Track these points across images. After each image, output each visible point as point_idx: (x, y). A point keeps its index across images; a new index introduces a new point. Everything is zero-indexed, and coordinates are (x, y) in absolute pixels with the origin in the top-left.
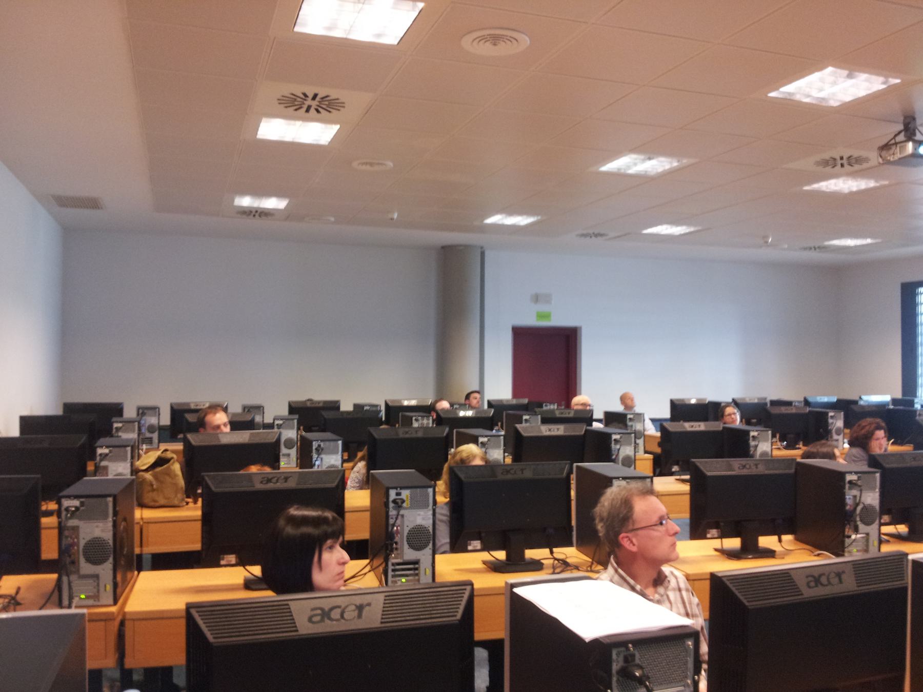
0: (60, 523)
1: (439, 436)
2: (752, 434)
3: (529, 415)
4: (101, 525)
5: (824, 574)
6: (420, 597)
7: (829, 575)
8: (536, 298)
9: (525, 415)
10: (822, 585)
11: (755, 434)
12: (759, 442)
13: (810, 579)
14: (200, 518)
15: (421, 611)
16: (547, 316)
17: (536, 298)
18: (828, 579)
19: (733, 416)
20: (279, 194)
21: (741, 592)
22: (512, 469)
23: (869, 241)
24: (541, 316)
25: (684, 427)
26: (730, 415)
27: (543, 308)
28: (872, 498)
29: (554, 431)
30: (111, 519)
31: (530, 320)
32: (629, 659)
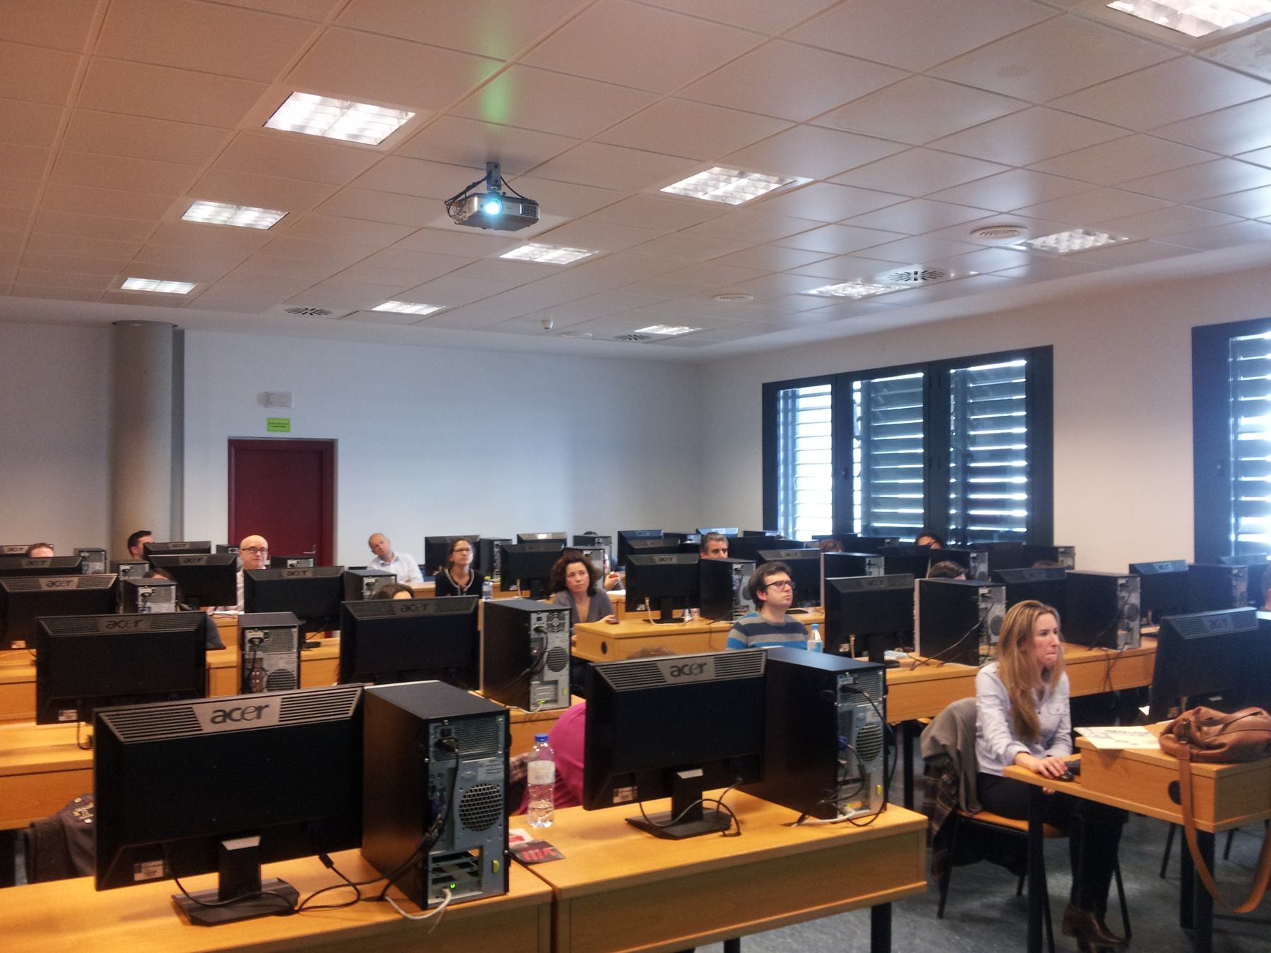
0: (243, 660)
1: (334, 576)
2: (735, 566)
3: (976, 552)
4: (284, 656)
5: (687, 665)
6: (147, 722)
7: (691, 666)
8: (267, 399)
9: (973, 552)
10: (685, 674)
11: (738, 566)
12: (743, 576)
13: (674, 669)
14: (823, 621)
15: (153, 735)
16: (284, 425)
17: (267, 399)
18: (691, 669)
19: (259, 553)
20: (265, 203)
21: (115, 725)
22: (413, 605)
23: (686, 330)
24: (273, 424)
25: (653, 560)
26: (461, 550)
27: (277, 413)
28: (1135, 599)
29: (298, 574)
30: (295, 651)
31: (256, 429)
32: (445, 733)
